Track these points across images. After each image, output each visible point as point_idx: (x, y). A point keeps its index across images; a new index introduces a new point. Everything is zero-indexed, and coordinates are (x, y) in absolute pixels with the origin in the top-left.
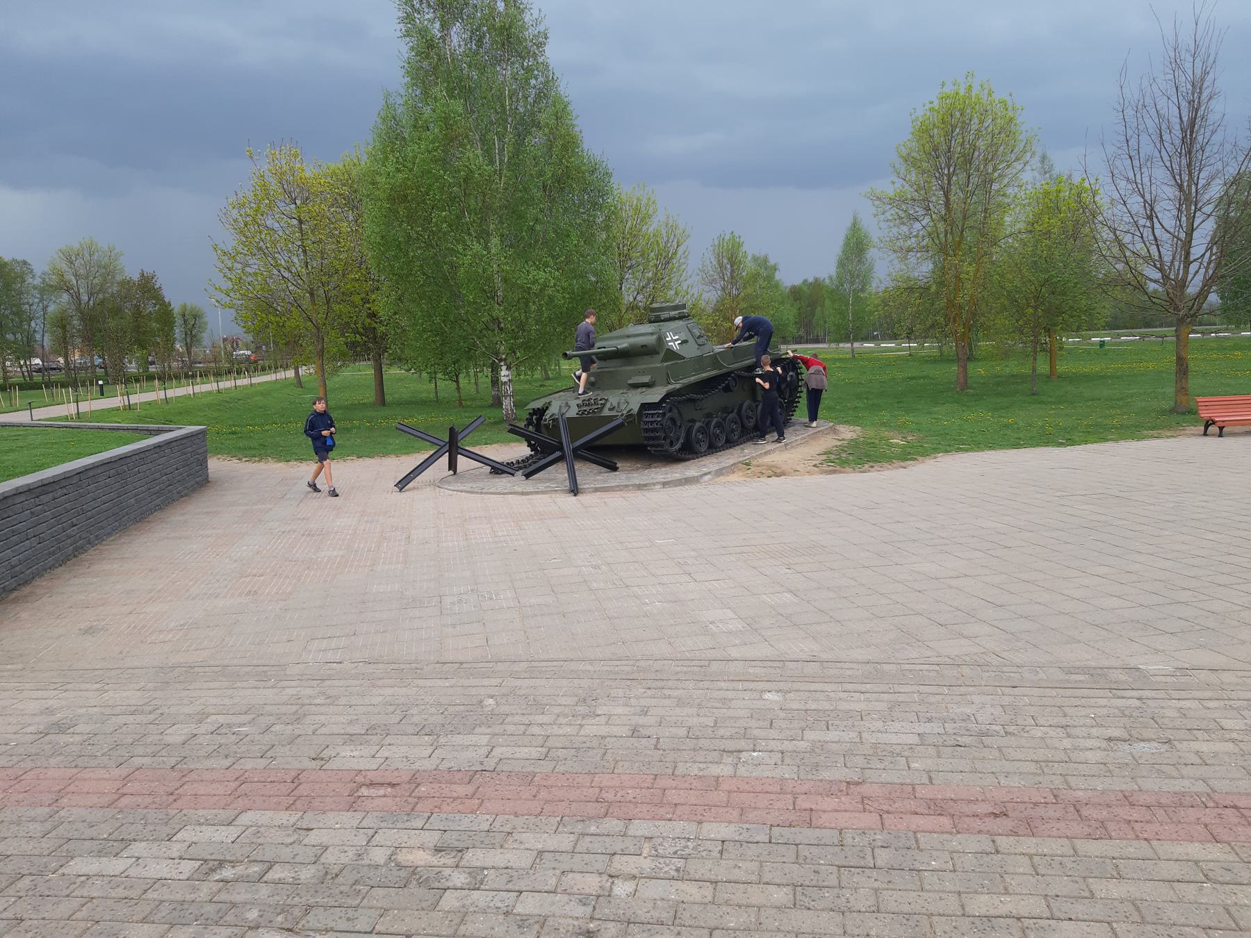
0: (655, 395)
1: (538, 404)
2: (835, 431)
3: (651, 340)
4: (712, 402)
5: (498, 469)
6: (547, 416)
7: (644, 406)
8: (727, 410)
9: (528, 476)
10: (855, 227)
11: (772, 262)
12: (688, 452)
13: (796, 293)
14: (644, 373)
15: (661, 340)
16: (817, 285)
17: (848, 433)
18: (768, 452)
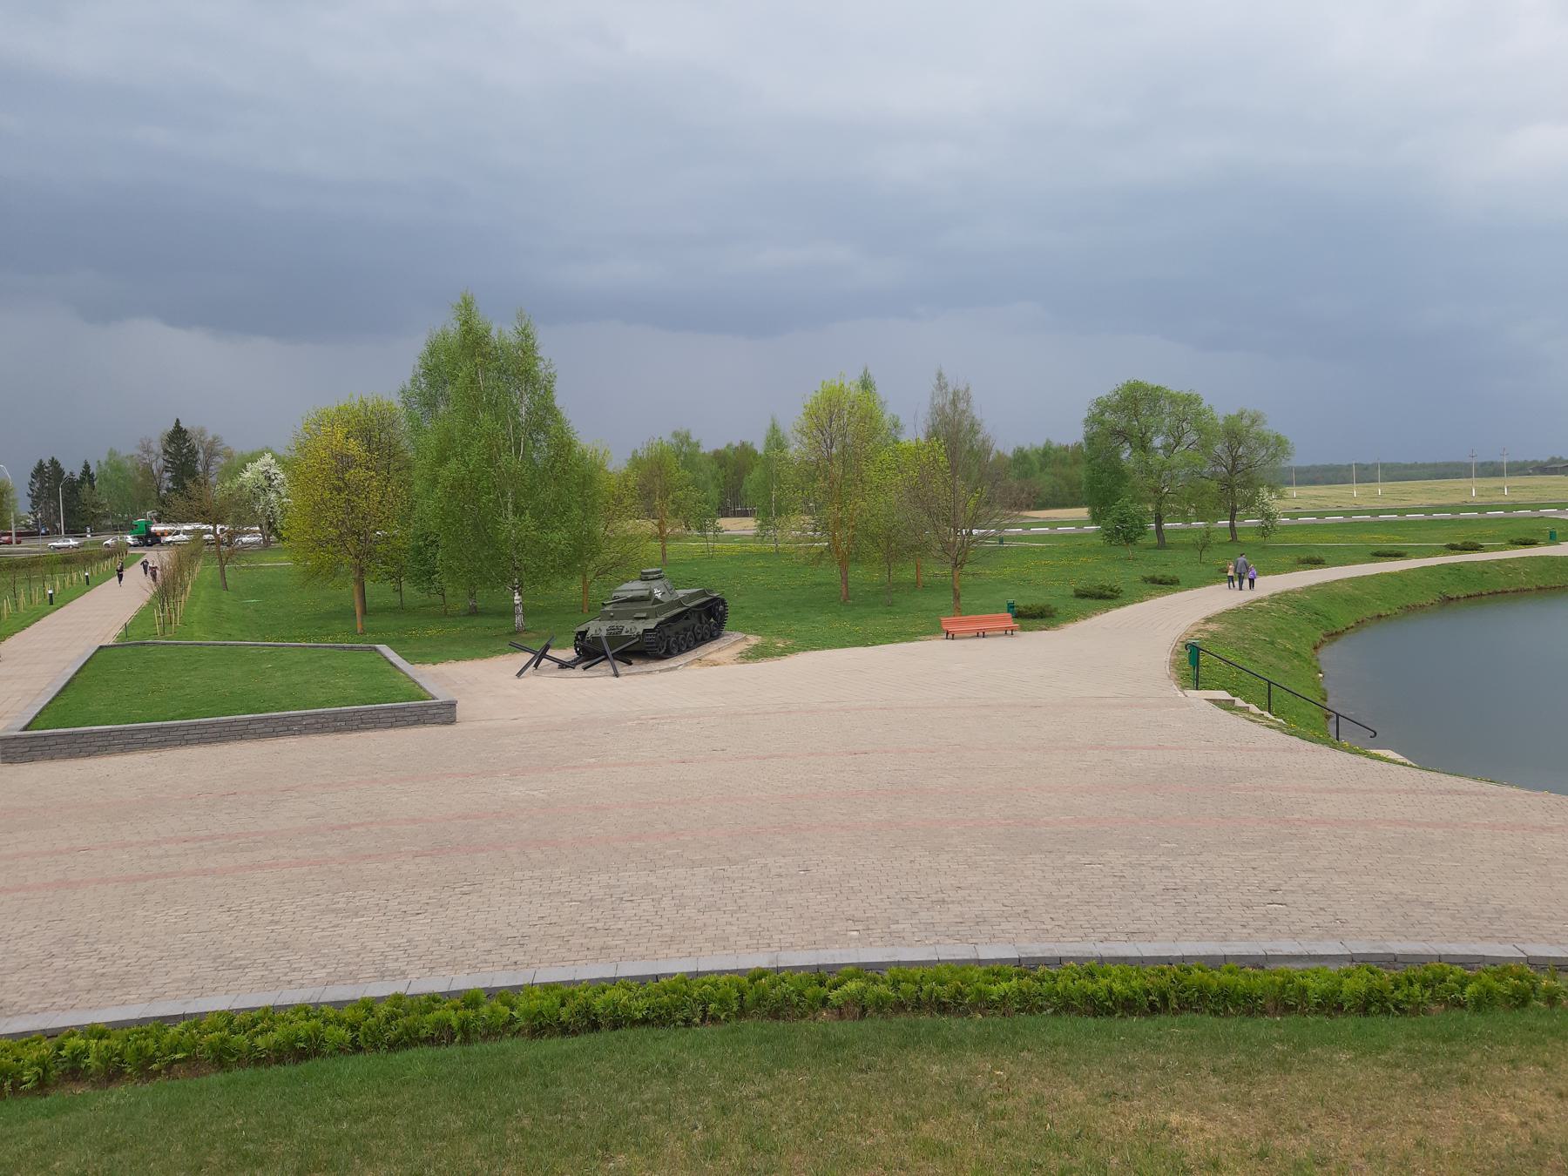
0: (651, 624)
1: (582, 629)
2: (745, 639)
4: (682, 624)
10: (774, 429)
11: (694, 440)
12: (668, 654)
13: (720, 458)
15: (651, 593)
16: (745, 450)
17: (754, 640)
18: (710, 650)
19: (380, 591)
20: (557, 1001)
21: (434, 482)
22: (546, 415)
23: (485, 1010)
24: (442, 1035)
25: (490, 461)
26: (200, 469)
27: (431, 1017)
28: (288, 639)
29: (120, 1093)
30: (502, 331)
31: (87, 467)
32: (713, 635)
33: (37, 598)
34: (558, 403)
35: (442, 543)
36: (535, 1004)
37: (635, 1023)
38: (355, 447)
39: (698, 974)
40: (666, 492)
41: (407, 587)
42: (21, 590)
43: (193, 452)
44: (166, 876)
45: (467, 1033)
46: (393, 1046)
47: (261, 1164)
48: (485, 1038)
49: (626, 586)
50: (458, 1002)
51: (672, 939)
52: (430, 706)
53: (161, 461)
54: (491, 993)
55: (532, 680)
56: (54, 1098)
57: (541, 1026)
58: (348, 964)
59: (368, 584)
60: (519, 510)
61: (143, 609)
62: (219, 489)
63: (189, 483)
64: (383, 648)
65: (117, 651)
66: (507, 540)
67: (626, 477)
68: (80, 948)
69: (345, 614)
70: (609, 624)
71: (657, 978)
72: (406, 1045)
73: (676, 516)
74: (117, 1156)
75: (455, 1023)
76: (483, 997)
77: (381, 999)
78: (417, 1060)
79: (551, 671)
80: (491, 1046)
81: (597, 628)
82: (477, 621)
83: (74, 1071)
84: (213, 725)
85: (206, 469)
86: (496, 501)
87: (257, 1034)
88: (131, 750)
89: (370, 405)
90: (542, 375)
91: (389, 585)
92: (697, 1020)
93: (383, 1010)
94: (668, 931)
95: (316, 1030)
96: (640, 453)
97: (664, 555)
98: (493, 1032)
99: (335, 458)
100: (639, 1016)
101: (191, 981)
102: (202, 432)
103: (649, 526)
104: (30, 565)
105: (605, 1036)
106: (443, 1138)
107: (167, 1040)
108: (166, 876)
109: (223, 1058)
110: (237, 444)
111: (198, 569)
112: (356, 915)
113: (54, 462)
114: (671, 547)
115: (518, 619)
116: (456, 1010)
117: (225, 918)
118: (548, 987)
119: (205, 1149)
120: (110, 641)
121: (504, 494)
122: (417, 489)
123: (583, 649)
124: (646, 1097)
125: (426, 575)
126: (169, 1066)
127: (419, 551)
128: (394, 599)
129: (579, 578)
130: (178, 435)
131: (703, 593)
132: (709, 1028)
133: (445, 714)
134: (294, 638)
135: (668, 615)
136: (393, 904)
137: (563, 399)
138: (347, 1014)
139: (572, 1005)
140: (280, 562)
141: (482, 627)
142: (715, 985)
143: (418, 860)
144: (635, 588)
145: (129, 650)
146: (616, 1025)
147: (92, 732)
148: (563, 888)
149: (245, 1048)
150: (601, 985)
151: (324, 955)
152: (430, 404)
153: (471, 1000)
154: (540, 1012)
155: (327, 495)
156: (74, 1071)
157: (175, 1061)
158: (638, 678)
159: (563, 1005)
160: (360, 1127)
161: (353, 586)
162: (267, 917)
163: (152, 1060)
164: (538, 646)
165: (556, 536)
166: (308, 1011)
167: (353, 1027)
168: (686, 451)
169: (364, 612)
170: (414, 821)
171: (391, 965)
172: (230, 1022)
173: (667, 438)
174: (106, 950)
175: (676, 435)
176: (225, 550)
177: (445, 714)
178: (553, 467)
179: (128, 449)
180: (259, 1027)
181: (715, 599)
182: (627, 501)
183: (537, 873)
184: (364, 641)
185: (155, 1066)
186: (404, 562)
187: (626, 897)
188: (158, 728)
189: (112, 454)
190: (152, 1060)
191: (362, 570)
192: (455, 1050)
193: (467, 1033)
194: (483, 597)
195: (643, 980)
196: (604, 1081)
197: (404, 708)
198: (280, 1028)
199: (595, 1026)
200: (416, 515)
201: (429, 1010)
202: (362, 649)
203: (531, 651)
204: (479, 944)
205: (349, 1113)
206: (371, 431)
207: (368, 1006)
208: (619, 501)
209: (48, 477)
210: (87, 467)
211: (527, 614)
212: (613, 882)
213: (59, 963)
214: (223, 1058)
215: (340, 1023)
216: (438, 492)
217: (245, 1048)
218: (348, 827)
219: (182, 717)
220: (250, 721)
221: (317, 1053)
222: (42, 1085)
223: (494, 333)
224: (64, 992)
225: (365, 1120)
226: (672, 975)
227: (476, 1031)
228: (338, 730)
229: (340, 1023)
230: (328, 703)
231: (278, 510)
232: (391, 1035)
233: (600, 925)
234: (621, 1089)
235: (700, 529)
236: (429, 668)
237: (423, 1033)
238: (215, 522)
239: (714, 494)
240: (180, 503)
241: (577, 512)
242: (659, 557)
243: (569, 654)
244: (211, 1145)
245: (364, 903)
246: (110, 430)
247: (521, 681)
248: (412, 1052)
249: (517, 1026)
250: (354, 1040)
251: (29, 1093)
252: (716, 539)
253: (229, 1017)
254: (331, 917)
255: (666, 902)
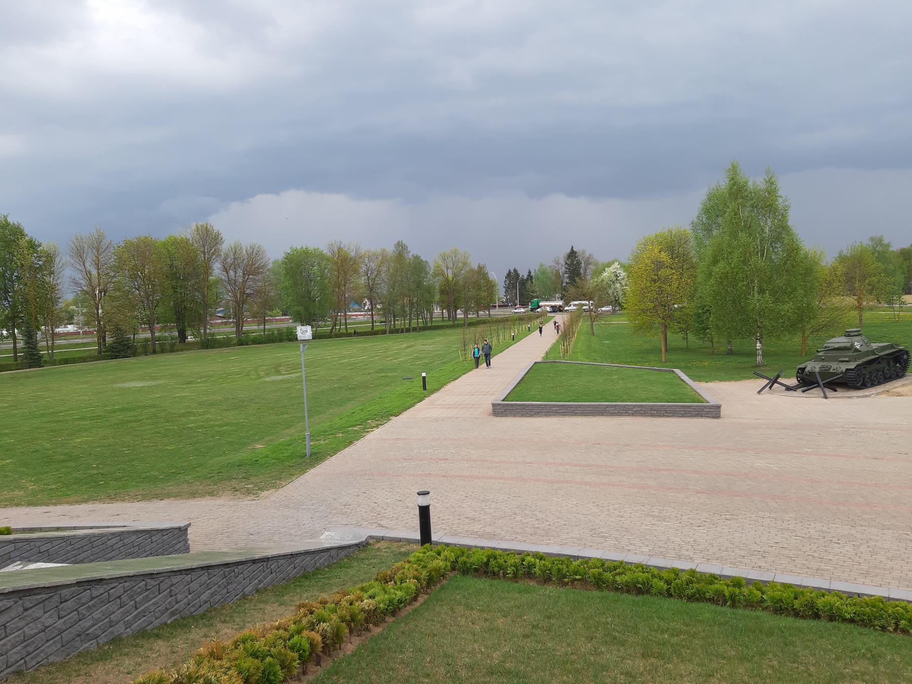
0: (852, 366)
1: (802, 366)
3: (849, 345)
4: (875, 366)
5: (788, 388)
6: (807, 370)
7: (847, 370)
8: (878, 370)
9: (803, 392)
11: (886, 242)
12: (864, 386)
14: (846, 357)
15: (852, 345)
19: (675, 339)
20: (792, 596)
21: (710, 275)
22: (782, 231)
23: (745, 590)
24: (718, 599)
25: (744, 262)
26: (582, 272)
27: (713, 587)
28: (625, 363)
29: (550, 589)
30: (756, 182)
31: (530, 272)
32: (898, 375)
33: (507, 337)
34: (790, 223)
35: (713, 310)
36: (777, 594)
37: (844, 620)
38: (664, 256)
39: (889, 599)
40: (863, 278)
41: (691, 337)
42: (501, 334)
43: (579, 263)
44: (567, 482)
45: (734, 601)
46: (691, 598)
47: (623, 645)
48: (745, 607)
49: (833, 340)
50: (729, 582)
51: (868, 573)
52: (705, 407)
53: (564, 269)
54: (749, 582)
55: (767, 396)
56: (521, 584)
57: (781, 608)
58: (660, 547)
59: (669, 334)
60: (761, 291)
61: (554, 345)
62: (591, 282)
63: (577, 279)
64: (677, 371)
65: (543, 365)
66: (753, 309)
67: (835, 269)
68: (527, 512)
69: (655, 351)
70: (820, 364)
71: (859, 595)
72: (698, 600)
73: (871, 293)
74: (552, 622)
75: (727, 594)
76: (744, 583)
77: (683, 571)
78: (706, 610)
79: (781, 391)
80: (748, 612)
81: (813, 366)
82: (733, 358)
83: (529, 573)
84: (588, 406)
85: (585, 272)
86: (747, 286)
87: (617, 574)
88: (549, 416)
89: (674, 232)
90: (780, 207)
91: (681, 335)
92: (891, 629)
93: (685, 577)
94: (865, 567)
95: (648, 579)
96: (845, 253)
97: (861, 320)
98: (750, 604)
99: (653, 263)
100: (848, 616)
101: (580, 539)
102: (584, 252)
103: (851, 300)
104: (504, 321)
105: (823, 624)
106: (724, 658)
107: (572, 568)
108: (567, 482)
109: (599, 583)
110: (600, 257)
111: (580, 324)
112: (664, 520)
113: (515, 271)
114: (867, 315)
115: (759, 358)
116: (728, 586)
117: (595, 510)
118: (786, 586)
119: (593, 629)
120: (539, 360)
121: (752, 281)
122: (699, 280)
123: (802, 379)
124: (857, 668)
125: (703, 330)
126: (572, 582)
127: (699, 316)
128: (683, 344)
129: (799, 334)
130: (572, 254)
131: (892, 346)
132: (899, 637)
133: (714, 412)
134: (629, 363)
135: (865, 360)
136: (685, 518)
137: (793, 221)
138: (664, 574)
139: (802, 600)
140: (621, 321)
141: (737, 362)
142: (905, 608)
143: (699, 495)
144: (840, 341)
145: (548, 365)
146: (831, 618)
147: (533, 405)
148: (791, 527)
149: (610, 581)
150: (822, 593)
151: (647, 539)
152: (708, 229)
153: (737, 583)
154: (781, 600)
155: (648, 284)
156: (529, 573)
157: (575, 580)
158: (841, 400)
159: (796, 598)
160: (674, 640)
161: (661, 336)
162: (617, 513)
163: (564, 576)
164: (773, 375)
165: (786, 307)
166: (644, 568)
167: (668, 582)
168: (879, 251)
169: (666, 350)
170: (696, 472)
171: (685, 553)
172: (603, 565)
173: (866, 242)
174: (540, 515)
175: (872, 239)
176: (593, 316)
177: (714, 412)
178: (785, 264)
179: (549, 263)
180: (618, 571)
181: (901, 350)
182: (835, 285)
183: (773, 515)
184: (666, 367)
185: (566, 580)
186: (690, 322)
187: (835, 540)
188: (563, 406)
189: (541, 265)
190: (564, 576)
191: (666, 326)
192: (726, 609)
193: (734, 601)
194: (736, 344)
195: (851, 595)
196: (825, 651)
197: (690, 406)
198: (628, 574)
199: (816, 616)
200: (698, 294)
201: (711, 583)
202: (665, 371)
203: (767, 378)
204: (737, 551)
205: (668, 629)
206: (674, 247)
207: (676, 572)
208: (830, 284)
209: (513, 277)
210: (530, 272)
211: (765, 355)
212: (825, 529)
213: (518, 518)
214: (599, 583)
215: (661, 578)
216: (712, 281)
217: (610, 581)
218: (659, 470)
219: (574, 401)
220: (607, 406)
221: (648, 592)
222: (515, 577)
223: (750, 184)
224: (521, 533)
225: (677, 635)
226: (871, 596)
227: (739, 602)
228: (652, 415)
229: (661, 578)
230: (647, 400)
231: (620, 293)
232: (689, 592)
233: (816, 555)
234: (837, 659)
235: (890, 302)
236: (703, 384)
237: (707, 595)
238: (589, 300)
239: (900, 278)
240: (572, 290)
241: (800, 291)
242: (857, 321)
243: (793, 382)
244: (597, 628)
245: (668, 514)
246: (541, 256)
247: (760, 396)
248: (701, 605)
249: (765, 605)
250: (668, 590)
251: (509, 579)
252: (901, 309)
253: (602, 563)
254: (650, 519)
255: (863, 548)
